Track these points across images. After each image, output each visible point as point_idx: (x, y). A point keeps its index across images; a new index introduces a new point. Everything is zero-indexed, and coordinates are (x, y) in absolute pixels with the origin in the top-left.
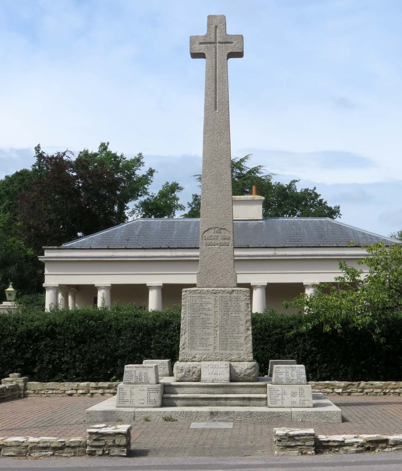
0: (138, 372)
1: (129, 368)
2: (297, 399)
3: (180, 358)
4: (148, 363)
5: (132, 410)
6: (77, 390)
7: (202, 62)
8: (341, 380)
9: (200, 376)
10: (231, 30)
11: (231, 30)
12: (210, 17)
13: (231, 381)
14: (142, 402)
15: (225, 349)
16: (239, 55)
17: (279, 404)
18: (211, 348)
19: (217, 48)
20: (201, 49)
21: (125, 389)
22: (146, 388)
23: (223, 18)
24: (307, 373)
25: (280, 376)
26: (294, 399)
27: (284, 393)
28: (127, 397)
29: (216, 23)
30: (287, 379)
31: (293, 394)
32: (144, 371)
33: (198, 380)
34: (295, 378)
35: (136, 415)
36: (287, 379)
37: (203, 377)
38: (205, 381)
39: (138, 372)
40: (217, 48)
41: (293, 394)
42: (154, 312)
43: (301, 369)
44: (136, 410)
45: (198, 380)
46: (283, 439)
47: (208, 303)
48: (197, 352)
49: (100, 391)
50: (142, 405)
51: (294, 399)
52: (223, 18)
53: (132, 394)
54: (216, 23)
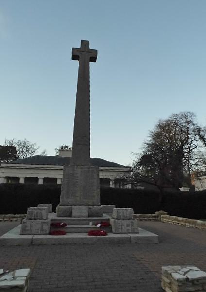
0: (36, 212)
1: (30, 209)
2: (129, 228)
3: (60, 204)
4: (40, 206)
5: (30, 237)
6: (4, 218)
7: (77, 62)
8: (180, 217)
9: (71, 213)
10: (92, 47)
11: (92, 47)
12: (82, 41)
13: (89, 216)
14: (37, 231)
15: (86, 199)
16: (95, 61)
17: (120, 231)
18: (78, 198)
19: (84, 55)
20: (78, 54)
21: (27, 222)
22: (40, 223)
23: (88, 42)
24: (134, 211)
25: (120, 215)
26: (129, 228)
27: (123, 225)
28: (28, 228)
29: (85, 43)
30: (124, 216)
31: (128, 225)
32: (39, 211)
33: (70, 216)
34: (128, 216)
35: (33, 241)
36: (124, 216)
37: (74, 214)
38: (74, 217)
39: (36, 212)
40: (84, 55)
41: (128, 225)
42: (73, 155)
43: (131, 210)
44: (34, 237)
45: (70, 216)
46: (184, 284)
47: (77, 173)
48: (70, 200)
49: (15, 219)
50: (38, 233)
51: (129, 228)
52: (88, 42)
53: (31, 226)
54: (85, 43)
